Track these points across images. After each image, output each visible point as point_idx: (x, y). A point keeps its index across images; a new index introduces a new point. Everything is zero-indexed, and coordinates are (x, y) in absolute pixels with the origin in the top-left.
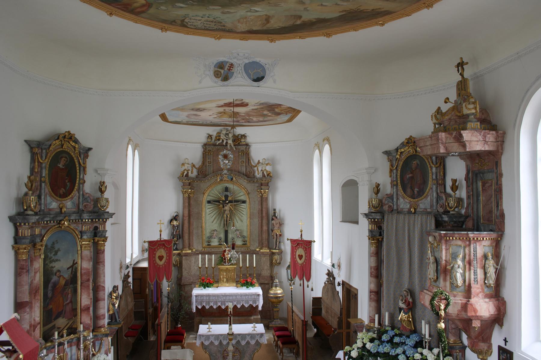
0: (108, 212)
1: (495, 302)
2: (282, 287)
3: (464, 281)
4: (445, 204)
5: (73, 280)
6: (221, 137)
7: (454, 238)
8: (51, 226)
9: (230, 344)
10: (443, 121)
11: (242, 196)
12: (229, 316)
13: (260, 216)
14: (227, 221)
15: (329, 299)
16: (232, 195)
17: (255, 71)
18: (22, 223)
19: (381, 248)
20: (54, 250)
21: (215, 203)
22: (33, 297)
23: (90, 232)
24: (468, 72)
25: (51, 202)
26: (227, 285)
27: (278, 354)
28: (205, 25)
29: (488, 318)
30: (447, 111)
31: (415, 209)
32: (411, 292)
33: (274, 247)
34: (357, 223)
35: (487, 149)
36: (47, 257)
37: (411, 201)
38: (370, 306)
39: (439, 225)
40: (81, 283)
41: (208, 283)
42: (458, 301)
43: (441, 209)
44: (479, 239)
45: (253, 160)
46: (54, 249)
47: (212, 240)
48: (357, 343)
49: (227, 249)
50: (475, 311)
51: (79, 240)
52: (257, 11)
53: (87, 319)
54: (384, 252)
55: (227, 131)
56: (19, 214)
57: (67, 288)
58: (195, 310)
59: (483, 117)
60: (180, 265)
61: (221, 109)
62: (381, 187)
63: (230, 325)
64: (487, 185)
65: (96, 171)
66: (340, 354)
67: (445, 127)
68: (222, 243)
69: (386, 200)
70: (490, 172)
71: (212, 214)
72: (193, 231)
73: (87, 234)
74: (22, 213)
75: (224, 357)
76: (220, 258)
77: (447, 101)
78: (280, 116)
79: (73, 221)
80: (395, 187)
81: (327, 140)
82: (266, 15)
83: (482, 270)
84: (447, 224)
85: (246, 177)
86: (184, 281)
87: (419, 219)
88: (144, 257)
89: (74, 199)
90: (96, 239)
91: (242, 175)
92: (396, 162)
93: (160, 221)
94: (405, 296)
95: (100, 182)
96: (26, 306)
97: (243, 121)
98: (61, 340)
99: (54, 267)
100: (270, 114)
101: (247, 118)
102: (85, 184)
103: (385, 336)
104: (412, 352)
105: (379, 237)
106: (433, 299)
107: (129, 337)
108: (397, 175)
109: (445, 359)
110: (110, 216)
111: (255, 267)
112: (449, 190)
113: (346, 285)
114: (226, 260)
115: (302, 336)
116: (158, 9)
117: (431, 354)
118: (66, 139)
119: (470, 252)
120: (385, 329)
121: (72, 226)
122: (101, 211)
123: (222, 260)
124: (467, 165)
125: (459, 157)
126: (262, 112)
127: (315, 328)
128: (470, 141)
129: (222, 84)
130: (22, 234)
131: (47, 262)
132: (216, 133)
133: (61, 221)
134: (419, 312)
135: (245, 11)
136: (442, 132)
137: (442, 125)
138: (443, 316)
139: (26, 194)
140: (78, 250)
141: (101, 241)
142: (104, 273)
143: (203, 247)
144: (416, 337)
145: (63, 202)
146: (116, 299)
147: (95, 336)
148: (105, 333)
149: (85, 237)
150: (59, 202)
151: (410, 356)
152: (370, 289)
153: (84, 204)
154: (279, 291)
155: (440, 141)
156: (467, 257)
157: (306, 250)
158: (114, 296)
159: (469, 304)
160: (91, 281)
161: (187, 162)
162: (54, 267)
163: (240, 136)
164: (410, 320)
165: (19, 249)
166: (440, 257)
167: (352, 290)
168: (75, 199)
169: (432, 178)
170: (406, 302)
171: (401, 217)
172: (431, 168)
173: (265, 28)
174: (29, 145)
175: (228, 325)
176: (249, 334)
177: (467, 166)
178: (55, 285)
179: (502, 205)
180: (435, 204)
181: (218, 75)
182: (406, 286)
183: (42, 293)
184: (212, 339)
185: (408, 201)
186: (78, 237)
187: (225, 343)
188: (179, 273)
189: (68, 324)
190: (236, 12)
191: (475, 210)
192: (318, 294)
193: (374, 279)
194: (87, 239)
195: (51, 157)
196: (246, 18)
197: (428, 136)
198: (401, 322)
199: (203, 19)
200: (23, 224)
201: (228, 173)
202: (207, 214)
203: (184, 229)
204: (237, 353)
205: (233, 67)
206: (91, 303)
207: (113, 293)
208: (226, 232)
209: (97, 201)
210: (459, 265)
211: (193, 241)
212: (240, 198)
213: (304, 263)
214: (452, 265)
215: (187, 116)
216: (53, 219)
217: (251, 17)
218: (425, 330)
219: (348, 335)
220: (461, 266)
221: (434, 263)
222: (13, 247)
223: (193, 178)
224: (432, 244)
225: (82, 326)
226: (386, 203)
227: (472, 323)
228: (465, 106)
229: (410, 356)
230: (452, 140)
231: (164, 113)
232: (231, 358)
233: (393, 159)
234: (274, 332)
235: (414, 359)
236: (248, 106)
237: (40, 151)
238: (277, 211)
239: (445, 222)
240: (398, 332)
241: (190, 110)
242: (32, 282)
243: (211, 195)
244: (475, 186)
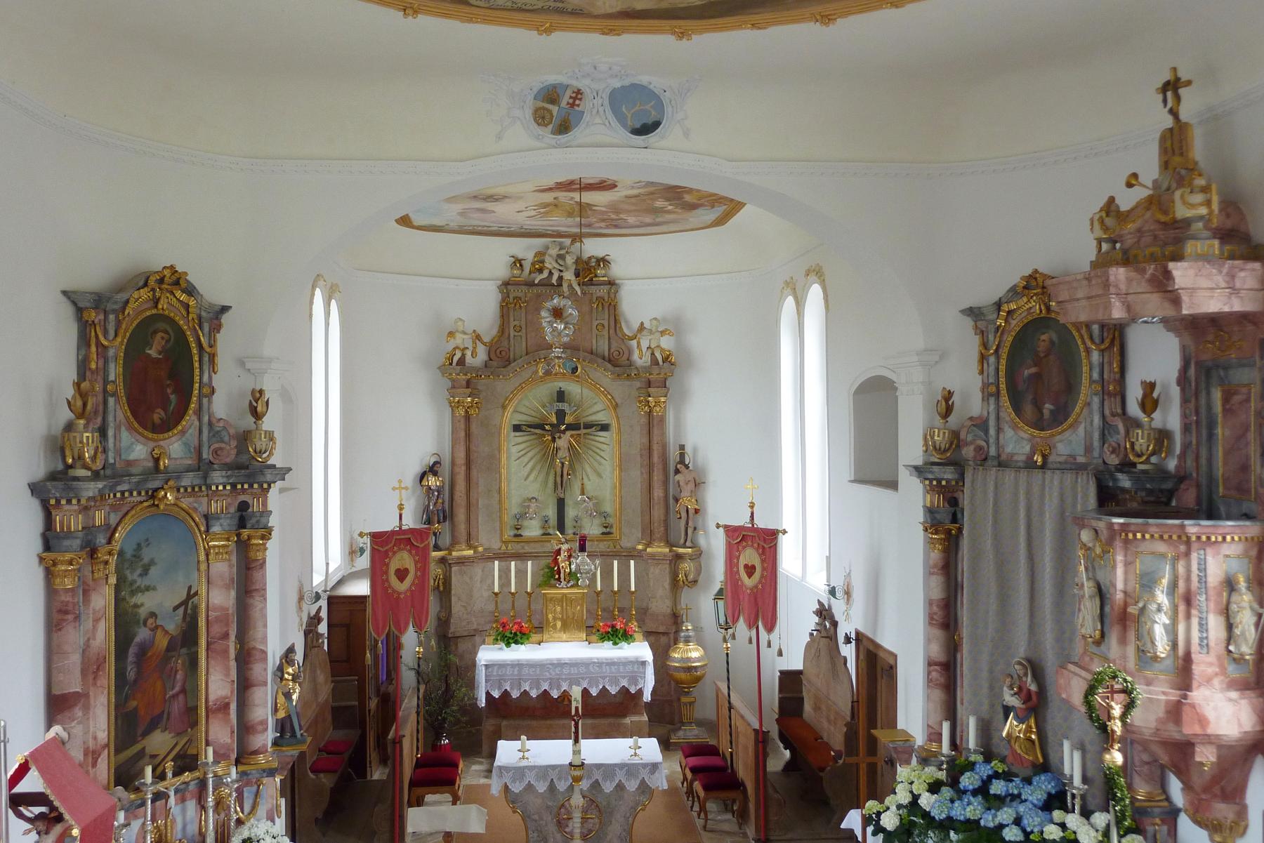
0: (273, 467)
1: (1255, 700)
2: (700, 643)
3: (1174, 645)
4: (1122, 444)
5: (188, 636)
6: (547, 265)
7: (1147, 536)
8: (132, 505)
9: (577, 789)
10: (1121, 236)
11: (598, 412)
12: (574, 720)
13: (645, 463)
14: (562, 476)
15: (821, 676)
16: (575, 411)
17: (637, 108)
18: (62, 498)
19: (957, 554)
21: (532, 430)
22: (91, 681)
23: (229, 515)
24: (1190, 106)
25: (132, 444)
26: (564, 636)
27: (695, 814)
29: (1237, 741)
30: (1132, 209)
31: (1044, 457)
32: (1035, 667)
33: (682, 541)
34: (892, 485)
36: (124, 582)
37: (1035, 437)
38: (928, 698)
39: (1108, 499)
40: (208, 644)
41: (515, 634)
42: (1156, 695)
43: (1113, 456)
44: (1213, 539)
45: (627, 322)
46: (141, 560)
47: (526, 523)
48: (895, 793)
49: (565, 547)
50: (1203, 721)
51: (202, 537)
53: (221, 733)
54: (965, 564)
55: (560, 249)
56: (53, 477)
58: (484, 701)
59: (1229, 224)
60: (444, 588)
61: (549, 197)
62: (955, 398)
63: (576, 741)
64: (1237, 398)
65: (241, 363)
66: (853, 820)
67: (1125, 252)
68: (551, 531)
69: (968, 433)
70: (1244, 366)
71: (526, 459)
73: (221, 521)
74: (60, 472)
75: (559, 822)
76: (547, 570)
77: (1132, 181)
79: (186, 490)
80: (992, 400)
81: (817, 273)
83: (1222, 620)
84: (1128, 497)
85: (609, 366)
86: (455, 628)
87: (1054, 481)
88: (354, 570)
89: (187, 435)
90: (245, 533)
91: (600, 360)
92: (995, 337)
93: (400, 481)
94: (1019, 676)
95: (253, 392)
96: (75, 705)
97: (603, 225)
98: (161, 787)
99: (142, 605)
100: (670, 207)
101: (613, 216)
102: (215, 397)
104: (1037, 820)
105: (952, 526)
106: (1091, 690)
107: (320, 772)
108: (997, 370)
109: (1124, 841)
110: (279, 476)
111: (633, 593)
112: (1134, 409)
113: (865, 642)
114: (562, 575)
115: (756, 771)
117: (1087, 827)
118: (165, 286)
119: (1189, 571)
120: (966, 760)
121: (185, 503)
122: (256, 463)
123: (552, 574)
124: (1184, 346)
125: (1162, 325)
127: (786, 749)
128: (1193, 289)
129: (553, 142)
131: (123, 593)
132: (533, 255)
133: (156, 490)
134: (1054, 717)
136: (1118, 264)
137: (1118, 245)
138: (1119, 733)
139: (69, 427)
140: (199, 562)
141: (256, 537)
142: (264, 616)
143: (504, 542)
144: (1049, 783)
145: (161, 443)
146: (293, 680)
147: (243, 774)
148: (265, 766)
149: (216, 529)
150: (152, 444)
151: (1032, 832)
152: (929, 657)
153: (212, 448)
154: (694, 653)
155: (1112, 290)
156: (1181, 584)
157: (763, 553)
158: (288, 674)
159: (1185, 704)
160: (233, 637)
161: (461, 329)
162: (142, 605)
163: (593, 260)
164: (1033, 737)
165: (55, 564)
166: (1110, 581)
167: (881, 654)
168: (191, 435)
169: (1091, 377)
170: (1021, 691)
171: (1009, 476)
172: (1088, 351)
174: (74, 303)
175: (571, 742)
176: (622, 766)
177: (1184, 349)
178: (144, 649)
180: (1096, 444)
181: (543, 118)
182: (1021, 652)
183: (113, 671)
184: (530, 777)
185: (1026, 436)
186: (200, 530)
187: (562, 786)
188: (441, 607)
189: (176, 744)
191: (1203, 461)
192: (795, 662)
193: (938, 633)
194: (223, 534)
195: (130, 331)
197: (1082, 276)
198: (1009, 742)
200: (63, 502)
201: (563, 355)
202: (513, 458)
204: (592, 814)
205: (580, 99)
206: (232, 692)
207: (285, 665)
208: (561, 504)
209: (246, 440)
210: (1159, 605)
211: (478, 527)
213: (760, 586)
214: (1141, 605)
215: (462, 214)
216: (138, 487)
218: (1072, 764)
219: (872, 770)
220: (1165, 608)
221: (1094, 596)
222: (41, 559)
223: (476, 369)
224: (1089, 549)
225: (210, 750)
227: (1193, 753)
228: (1182, 197)
230: (1144, 286)
231: (407, 215)
232: (579, 825)
233: (987, 327)
234: (683, 757)
235: (1044, 839)
236: (616, 189)
237: (102, 317)
238: (688, 450)
239: (1124, 490)
240: (1000, 768)
241: (470, 198)
242: (87, 645)
243: (523, 410)
244: (1203, 401)
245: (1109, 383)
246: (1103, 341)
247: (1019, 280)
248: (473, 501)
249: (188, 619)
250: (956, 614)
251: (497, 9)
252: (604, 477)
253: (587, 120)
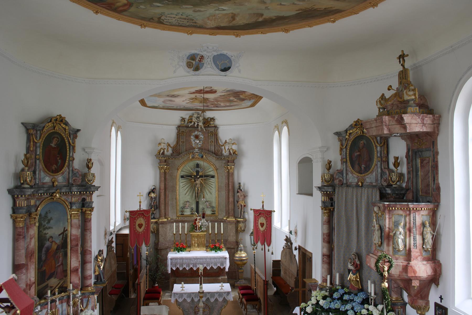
0: (94, 186)
1: (432, 264)
2: (246, 251)
3: (405, 246)
4: (388, 178)
5: (64, 245)
6: (193, 120)
7: (396, 209)
8: (44, 198)
9: (201, 301)
10: (386, 106)
11: (211, 171)
12: (200, 277)
13: (227, 189)
14: (198, 193)
15: (287, 262)
16: (202, 171)
17: (223, 62)
18: (20, 195)
19: (333, 217)
20: (47, 219)
21: (188, 177)
22: (29, 260)
23: (78, 203)
24: (408, 63)
25: (45, 177)
26: (198, 249)
27: (243, 310)
28: (179, 22)
29: (426, 278)
30: (390, 97)
31: (362, 183)
32: (359, 256)
33: (239, 216)
34: (311, 195)
35: (425, 130)
36: (41, 225)
37: (359, 176)
38: (323, 267)
39: (383, 197)
40: (71, 248)
41: (181, 248)
42: (399, 263)
43: (385, 182)
44: (418, 209)
45: (221, 140)
46: (47, 218)
47: (185, 210)
48: (311, 300)
49: (198, 218)
50: (415, 272)
51: (69, 210)
52: (224, 10)
53: (76, 279)
54: (335, 221)
55: (198, 115)
56: (16, 187)
57: (58, 252)
58: (170, 271)
59: (422, 103)
60: (157, 232)
61: (193, 96)
62: (332, 163)
63: (201, 284)
64: (425, 162)
65: (84, 150)
66: (297, 310)
67: (388, 111)
68: (194, 213)
69: (336, 175)
70: (427, 151)
71: (185, 188)
72: (168, 202)
73: (76, 205)
74: (19, 186)
75: (195, 312)
76: (192, 226)
77: (390, 88)
78: (244, 101)
79: (63, 193)
80: (344, 164)
81: (286, 122)
82: (232, 13)
83: (421, 237)
84: (390, 196)
85: (214, 155)
86: (160, 246)
87: (365, 192)
88: (125, 225)
89: (64, 174)
90: (84, 209)
91: (211, 153)
92: (345, 142)
93: (140, 193)
94: (353, 259)
95: (88, 160)
96: (23, 268)
97: (212, 106)
98: (54, 298)
99: (48, 233)
100: (235, 100)
101: (216, 103)
102: (74, 161)
103: (336, 294)
104: (359, 308)
105: (331, 208)
106: (377, 262)
107: (112, 295)
108: (346, 153)
109: (388, 314)
110: (96, 189)
111: (222, 234)
112: (391, 166)
113: (302, 249)
114: (197, 228)
115: (264, 294)
116: (137, 8)
117: (376, 310)
118: (57, 122)
119: (410, 220)
120: (336, 288)
121: (63, 198)
122: (88, 184)
123: (194, 227)
124: (408, 145)
125: (400, 137)
126: (228, 98)
127: (275, 287)
128: (410, 123)
129: (193, 74)
130: (19, 205)
131: (41, 229)
132: (188, 116)
133: (53, 193)
134: (365, 273)
135: (213, 10)
136: (386, 115)
137: (386, 110)
138: (387, 276)
139: (23, 170)
140: (68, 219)
141: (88, 211)
142: (91, 239)
143: (177, 216)
144: (363, 295)
145: (55, 177)
146: (101, 261)
147: (83, 294)
148: (92, 291)
149: (74, 207)
150: (52, 177)
151: (357, 312)
152: (323, 253)
153: (73, 179)
154: (244, 255)
155: (384, 124)
156: (408, 225)
157: (267, 219)
158: (99, 259)
159: (409, 266)
160: (80, 246)
161: (163, 142)
162: (48, 233)
163: (209, 119)
164: (358, 280)
165: (16, 218)
166: (384, 225)
167: (307, 253)
168: (66, 174)
169: (377, 155)
170: (354, 264)
171: (350, 190)
172: (376, 147)
173: (231, 24)
174: (26, 127)
175: (199, 285)
176: (217, 293)
177: (407, 145)
178: (48, 249)
179: (438, 179)
180: (379, 178)
181: (190, 65)
182: (354, 250)
183: (37, 257)
184: (185, 297)
185: (356, 176)
186: (68, 208)
187: (196, 300)
188: (156, 239)
189: (59, 283)
190: (206, 10)
191: (414, 184)
192: (278, 257)
193: (326, 245)
194: (76, 209)
195: (45, 137)
196: (215, 15)
197: (374, 119)
198: (350, 282)
199: (177, 17)
200: (20, 196)
201: (199, 152)
202: (181, 187)
203: (161, 201)
204: (207, 309)
205: (203, 59)
206: (79, 265)
207: (98, 256)
208: (197, 203)
209: (85, 176)
210: (400, 232)
211: (168, 211)
212: (209, 173)
213: (266, 231)
214: (394, 232)
215: (164, 102)
216: (46, 192)
217: (219, 15)
218: (371, 288)
219: (304, 293)
220: (402, 233)
221: (379, 230)
222: (11, 216)
223: (168, 156)
224: (377, 214)
225: (71, 285)
226: (337, 178)
227: (412, 283)
228: (406, 93)
229: (357, 312)
230: (394, 123)
231: (143, 99)
232: (202, 313)
233: (343, 139)
234: (239, 290)
235: (362, 314)
236: (217, 93)
237: (35, 132)
238: (242, 184)
239: (388, 194)
240: (347, 291)
241: (166, 96)
242: (28, 247)
243: (185, 170)
244: (414, 163)
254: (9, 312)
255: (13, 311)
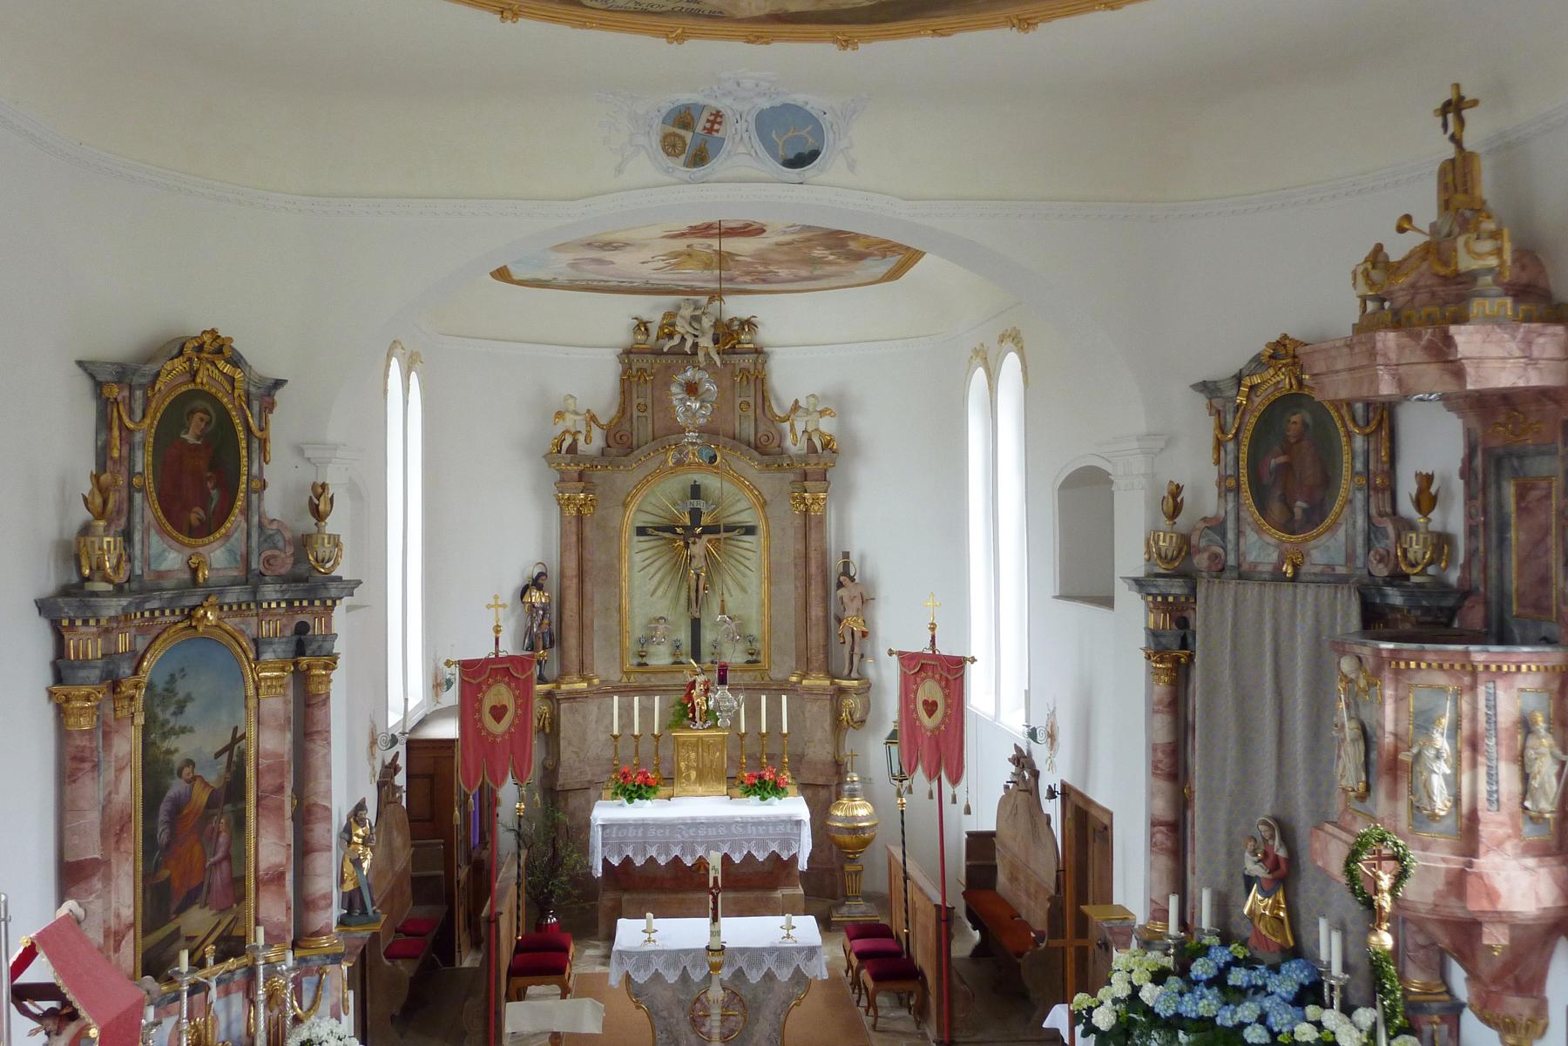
0: (339, 579)
1: (1556, 869)
2: (869, 798)
3: (1457, 801)
4: (1392, 551)
5: (234, 789)
6: (678, 329)
7: (1423, 665)
8: (164, 626)
9: (715, 979)
10: (1391, 293)
11: (742, 511)
12: (712, 894)
13: (800, 574)
14: (697, 590)
15: (1019, 839)
16: (714, 510)
17: (790, 134)
18: (77, 618)
19: (1187, 687)
21: (660, 533)
22: (113, 845)
23: (284, 640)
24: (1476, 131)
25: (164, 551)
26: (700, 790)
27: (862, 1010)
29: (1534, 920)
30: (1405, 260)
31: (1296, 567)
32: (1284, 828)
33: (846, 671)
34: (1107, 601)
36: (154, 722)
37: (1284, 542)
38: (1151, 866)
39: (1375, 619)
40: (258, 799)
41: (639, 786)
42: (1434, 862)
43: (1381, 566)
44: (1505, 668)
45: (778, 400)
46: (175, 695)
47: (652, 649)
48: (1111, 984)
49: (701, 679)
50: (1492, 895)
51: (250, 666)
53: (275, 909)
54: (1197, 700)
55: (695, 309)
56: (66, 591)
58: (600, 870)
59: (1524, 278)
60: (551, 730)
61: (680, 245)
62: (1185, 494)
63: (715, 919)
64: (1534, 494)
65: (299, 450)
66: (1058, 1018)
67: (1396, 312)
68: (683, 659)
69: (1201, 537)
70: (1543, 454)
71: (652, 570)
73: (274, 646)
74: (74, 586)
75: (693, 1020)
76: (678, 708)
77: (1405, 224)
79: (231, 608)
80: (1231, 496)
81: (1014, 338)
83: (1515, 769)
84: (1399, 616)
85: (756, 454)
86: (565, 779)
87: (1307, 597)
88: (439, 707)
89: (232, 540)
90: (304, 661)
91: (744, 447)
92: (1234, 418)
93: (496, 597)
94: (1264, 838)
95: (314, 486)
96: (93, 875)
97: (748, 279)
98: (199, 976)
99: (176, 750)
100: (831, 257)
101: (761, 269)
102: (266, 492)
104: (1287, 1017)
105: (1181, 653)
106: (1353, 857)
107: (397, 958)
108: (1237, 459)
109: (1394, 1043)
110: (346, 591)
111: (785, 735)
112: (1406, 507)
113: (1073, 796)
114: (697, 714)
115: (937, 956)
117: (1349, 1026)
118: (204, 355)
119: (1474, 709)
120: (1199, 943)
121: (229, 624)
122: (318, 575)
123: (685, 713)
124: (1468, 429)
125: (1441, 403)
127: (975, 929)
128: (1480, 358)
129: (686, 177)
131: (153, 736)
132: (662, 316)
133: (193, 608)
134: (1308, 890)
136: (1386, 327)
137: (1387, 305)
138: (1388, 909)
139: (86, 530)
140: (246, 697)
141: (317, 667)
142: (328, 765)
143: (625, 673)
144: (1302, 972)
145: (200, 550)
146: (364, 844)
147: (301, 961)
148: (328, 951)
149: (268, 656)
150: (188, 551)
151: (1280, 1032)
152: (1153, 815)
153: (263, 555)
154: (861, 810)
155: (1380, 360)
156: (1466, 725)
157: (947, 686)
158: (358, 836)
159: (1470, 874)
160: (288, 791)
161: (572, 408)
162: (176, 750)
163: (736, 323)
164: (1282, 914)
165: (68, 700)
166: (1377, 721)
167: (1093, 812)
168: (237, 539)
169: (1353, 467)
170: (1267, 858)
171: (1251, 591)
172: (1349, 435)
174: (92, 376)
175: (708, 921)
176: (771, 950)
177: (1468, 433)
178: (178, 806)
180: (1360, 550)
181: (674, 146)
182: (1267, 809)
183: (141, 833)
184: (658, 965)
185: (1272, 541)
186: (248, 658)
187: (697, 975)
188: (548, 753)
189: (218, 924)
191: (1493, 572)
192: (986, 821)
193: (1164, 785)
194: (276, 663)
195: (161, 411)
197: (1342, 342)
198: (1252, 920)
200: (79, 623)
201: (698, 441)
202: (637, 569)
204: (734, 1010)
205: (720, 123)
206: (288, 859)
207: (354, 825)
208: (696, 625)
209: (305, 546)
210: (1438, 751)
211: (593, 654)
213: (943, 728)
214: (1415, 750)
215: (573, 265)
216: (171, 604)
218: (1330, 948)
219: (1082, 955)
220: (1445, 755)
221: (1357, 740)
222: (51, 694)
223: (591, 458)
224: (1351, 681)
225: (261, 931)
227: (1480, 934)
228: (1466, 244)
230: (1419, 355)
231: (505, 267)
232: (718, 1024)
233: (1224, 406)
234: (847, 939)
235: (1295, 1041)
236: (764, 235)
237: (126, 393)
238: (854, 558)
239: (1394, 608)
240: (1241, 953)
241: (583, 245)
242: (108, 800)
243: (649, 509)
244: (1492, 498)
245: (1376, 475)
246: (1368, 424)
247: (1264, 347)
248: (587, 621)
249: (233, 768)
250: (1186, 762)
251: (616, 11)
252: (750, 591)
253: (728, 148)
254: (58, 1033)
255: (72, 1029)
